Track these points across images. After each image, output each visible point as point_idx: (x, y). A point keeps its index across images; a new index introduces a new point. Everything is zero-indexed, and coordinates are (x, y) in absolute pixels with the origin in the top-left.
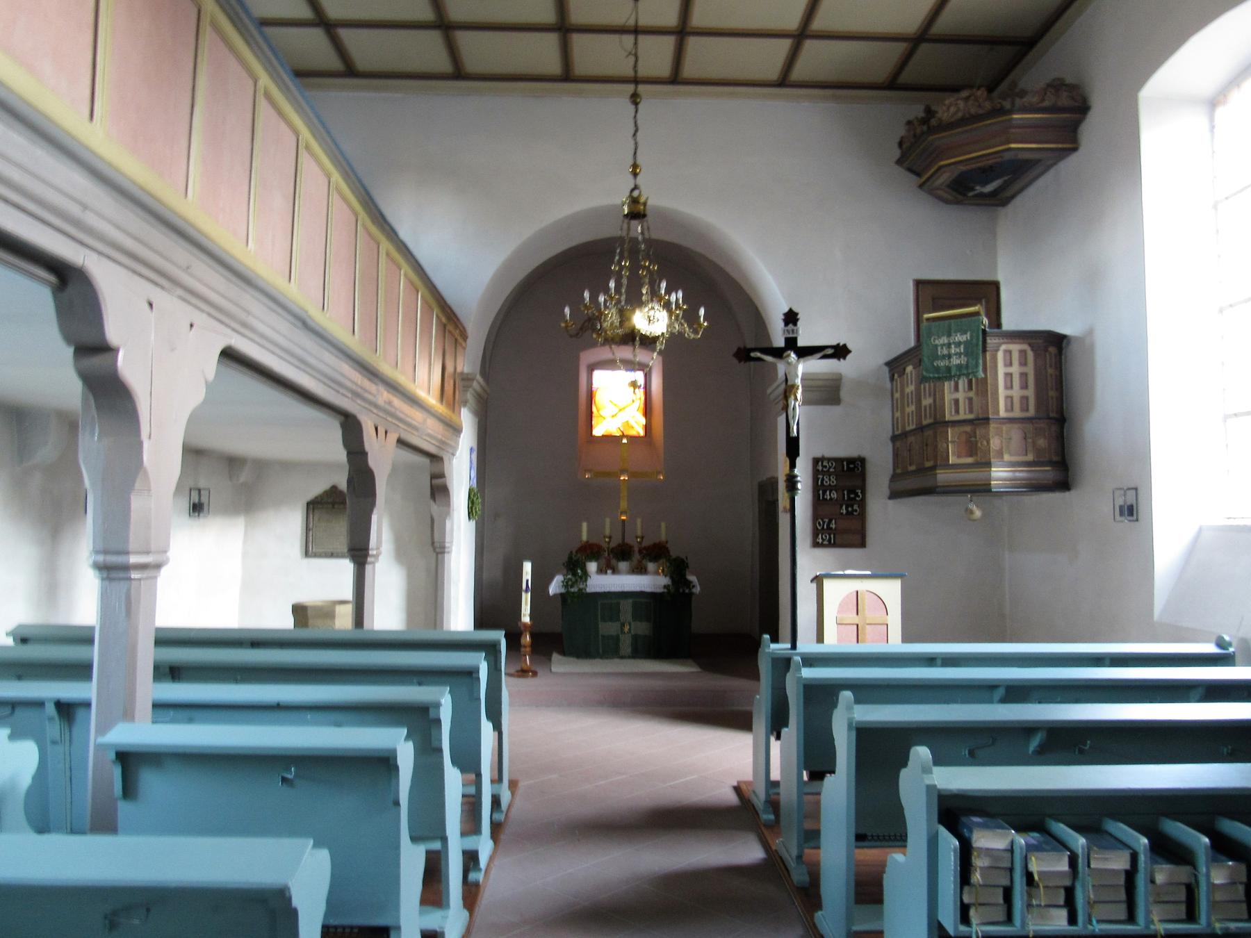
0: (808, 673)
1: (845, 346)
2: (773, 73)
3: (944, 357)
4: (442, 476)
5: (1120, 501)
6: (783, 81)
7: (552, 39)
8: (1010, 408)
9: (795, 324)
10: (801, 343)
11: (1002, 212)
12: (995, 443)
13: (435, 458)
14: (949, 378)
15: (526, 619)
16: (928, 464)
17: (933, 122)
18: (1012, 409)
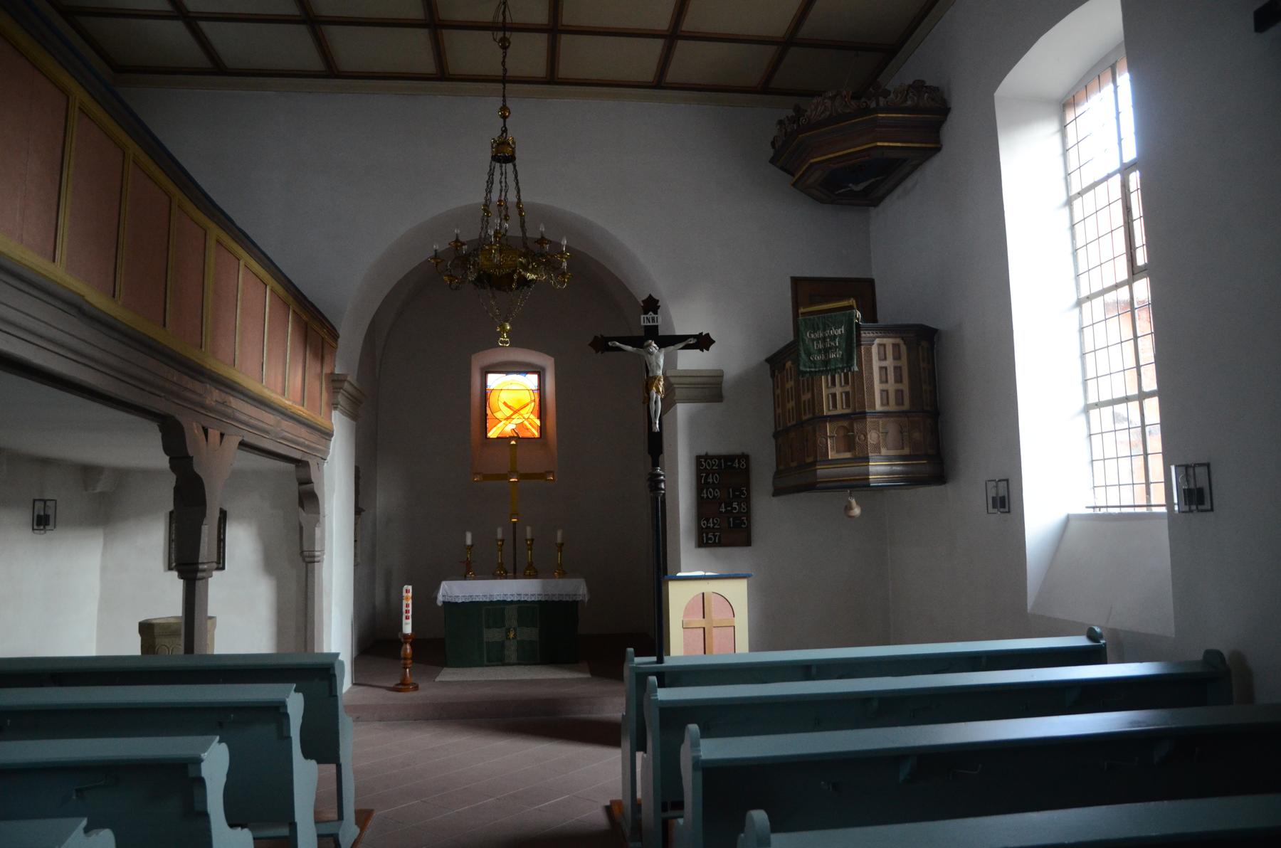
0: (664, 694)
1: (708, 335)
2: (649, 77)
3: (819, 351)
4: (309, 482)
5: (992, 493)
6: (659, 83)
7: (422, 35)
8: (885, 401)
9: (656, 313)
11: (873, 211)
12: (873, 437)
13: (301, 464)
14: (826, 372)
15: (408, 628)
16: (810, 460)
17: (802, 120)
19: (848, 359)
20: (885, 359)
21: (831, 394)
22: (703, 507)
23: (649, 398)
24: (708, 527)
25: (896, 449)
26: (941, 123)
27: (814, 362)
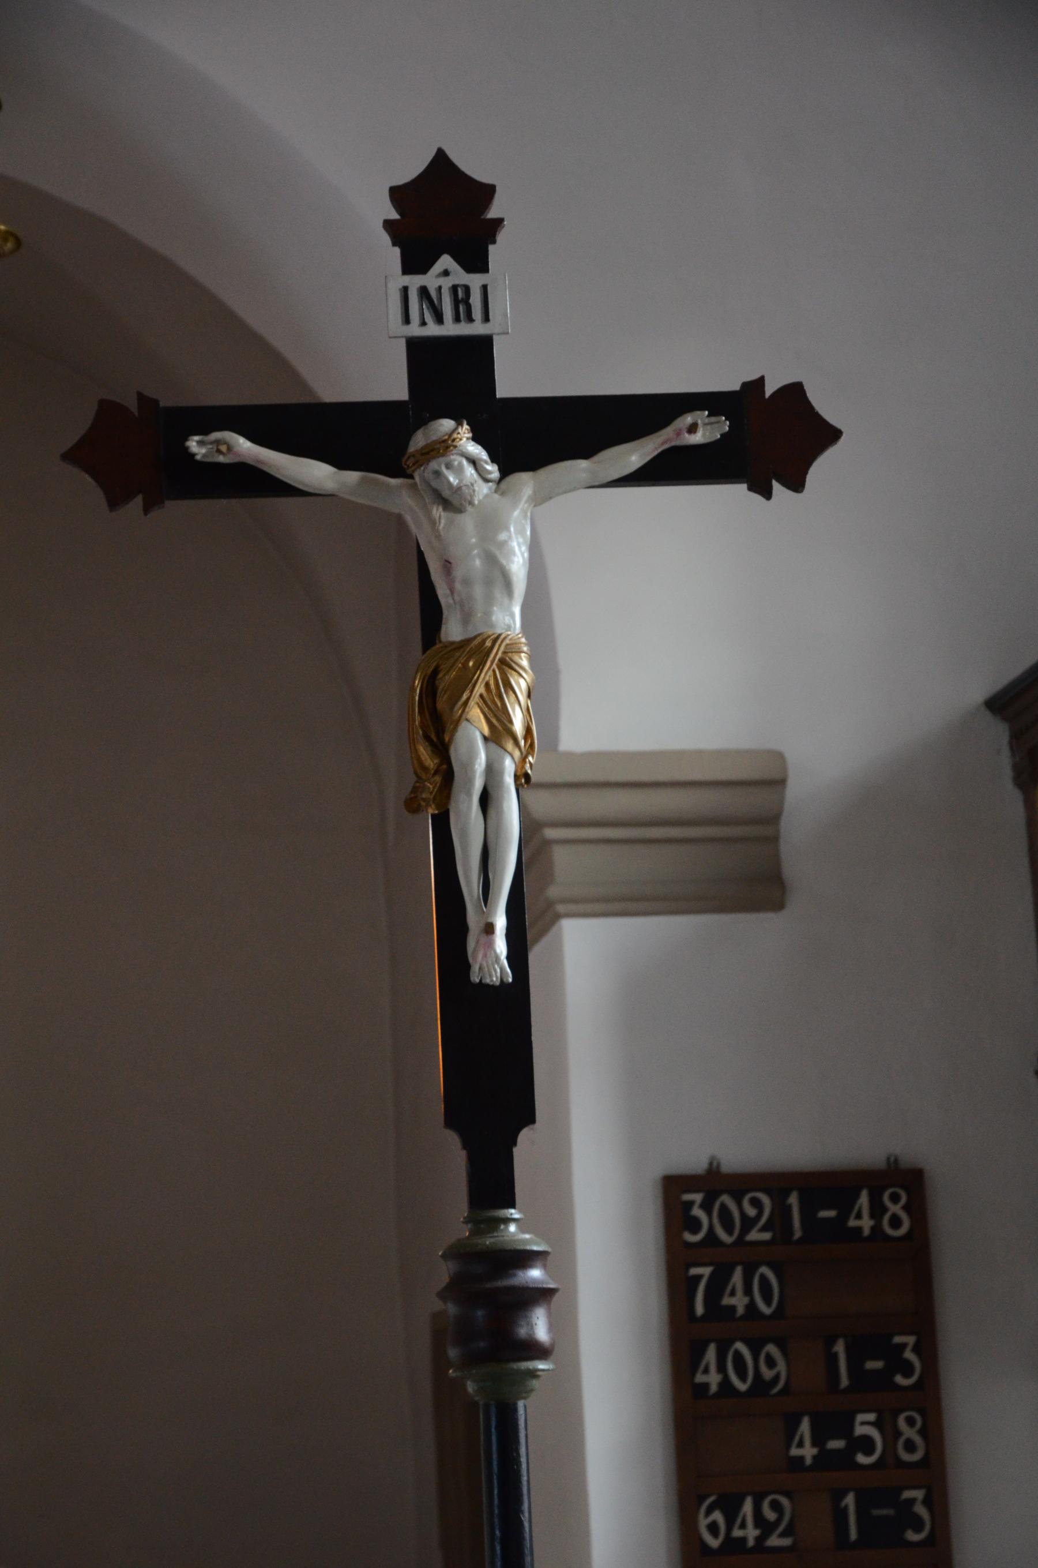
9: (475, 260)
10: (514, 379)
23: (447, 776)
24: (733, 1546)
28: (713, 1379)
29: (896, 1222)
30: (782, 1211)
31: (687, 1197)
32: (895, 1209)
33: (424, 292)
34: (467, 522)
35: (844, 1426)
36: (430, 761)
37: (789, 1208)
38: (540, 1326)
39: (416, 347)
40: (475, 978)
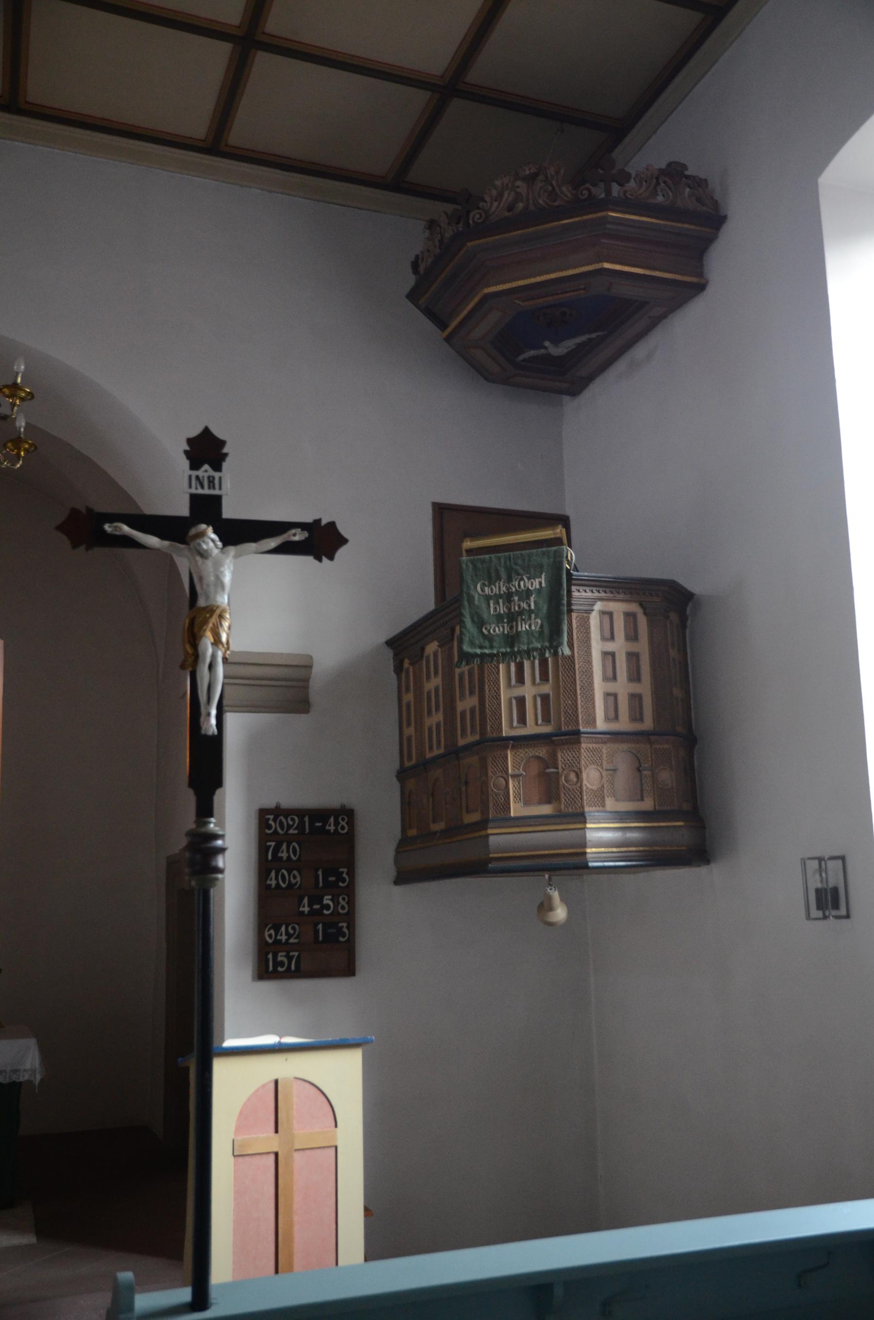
1: (332, 525)
3: (499, 618)
5: (815, 882)
6: (215, 144)
8: (613, 715)
9: (217, 467)
10: (228, 512)
11: (570, 404)
12: (591, 778)
16: (475, 817)
17: (475, 216)
18: (617, 717)
19: (553, 631)
20: (612, 638)
21: (516, 697)
22: (270, 904)
23: (196, 657)
24: (277, 942)
25: (631, 799)
26: (710, 240)
27: (489, 638)
28: (273, 883)
29: (343, 828)
30: (302, 822)
31: (267, 817)
32: (344, 823)
33: (197, 477)
34: (209, 563)
35: (320, 900)
36: (190, 650)
37: (305, 822)
38: (220, 862)
39: (194, 498)
40: (203, 732)
